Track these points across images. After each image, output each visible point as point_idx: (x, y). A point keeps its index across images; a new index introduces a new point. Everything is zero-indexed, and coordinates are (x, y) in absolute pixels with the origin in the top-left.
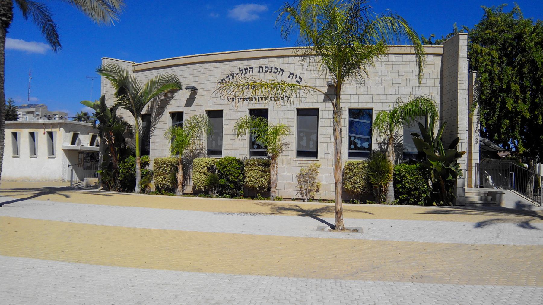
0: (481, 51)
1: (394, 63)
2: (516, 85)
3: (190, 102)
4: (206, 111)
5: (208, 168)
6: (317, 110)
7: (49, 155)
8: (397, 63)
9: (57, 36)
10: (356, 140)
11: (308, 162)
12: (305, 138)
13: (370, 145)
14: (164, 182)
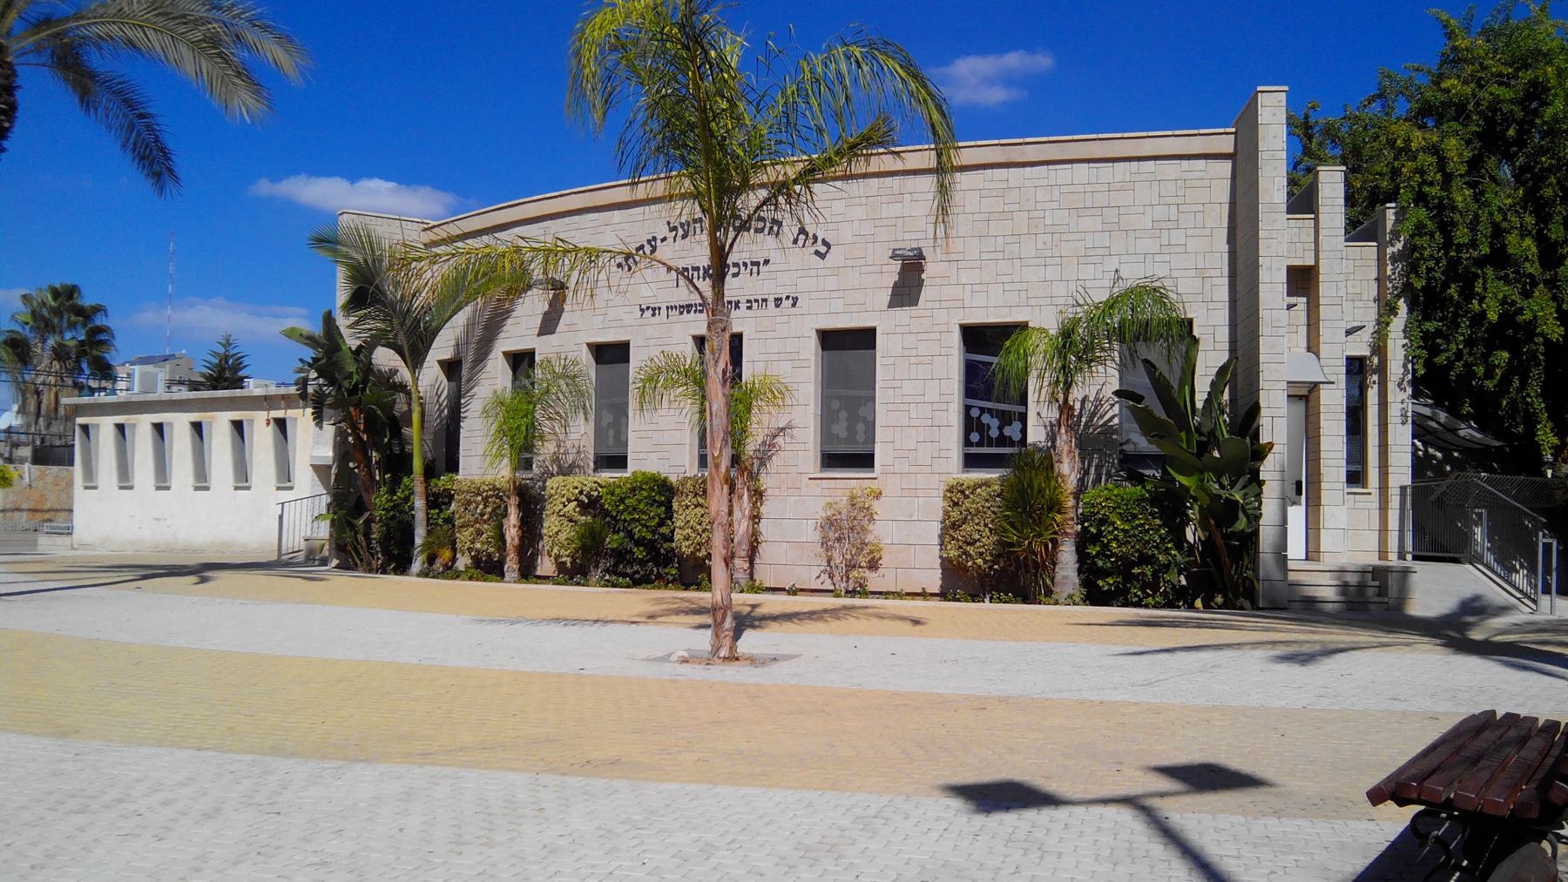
0: (1408, 141)
1: (1088, 188)
2: (1528, 241)
3: (549, 325)
4: (589, 345)
5: (581, 504)
6: (871, 332)
7: (279, 481)
8: (1097, 187)
9: (165, 153)
10: (986, 419)
11: (849, 481)
12: (843, 415)
13: (1024, 431)
14: (478, 546)
